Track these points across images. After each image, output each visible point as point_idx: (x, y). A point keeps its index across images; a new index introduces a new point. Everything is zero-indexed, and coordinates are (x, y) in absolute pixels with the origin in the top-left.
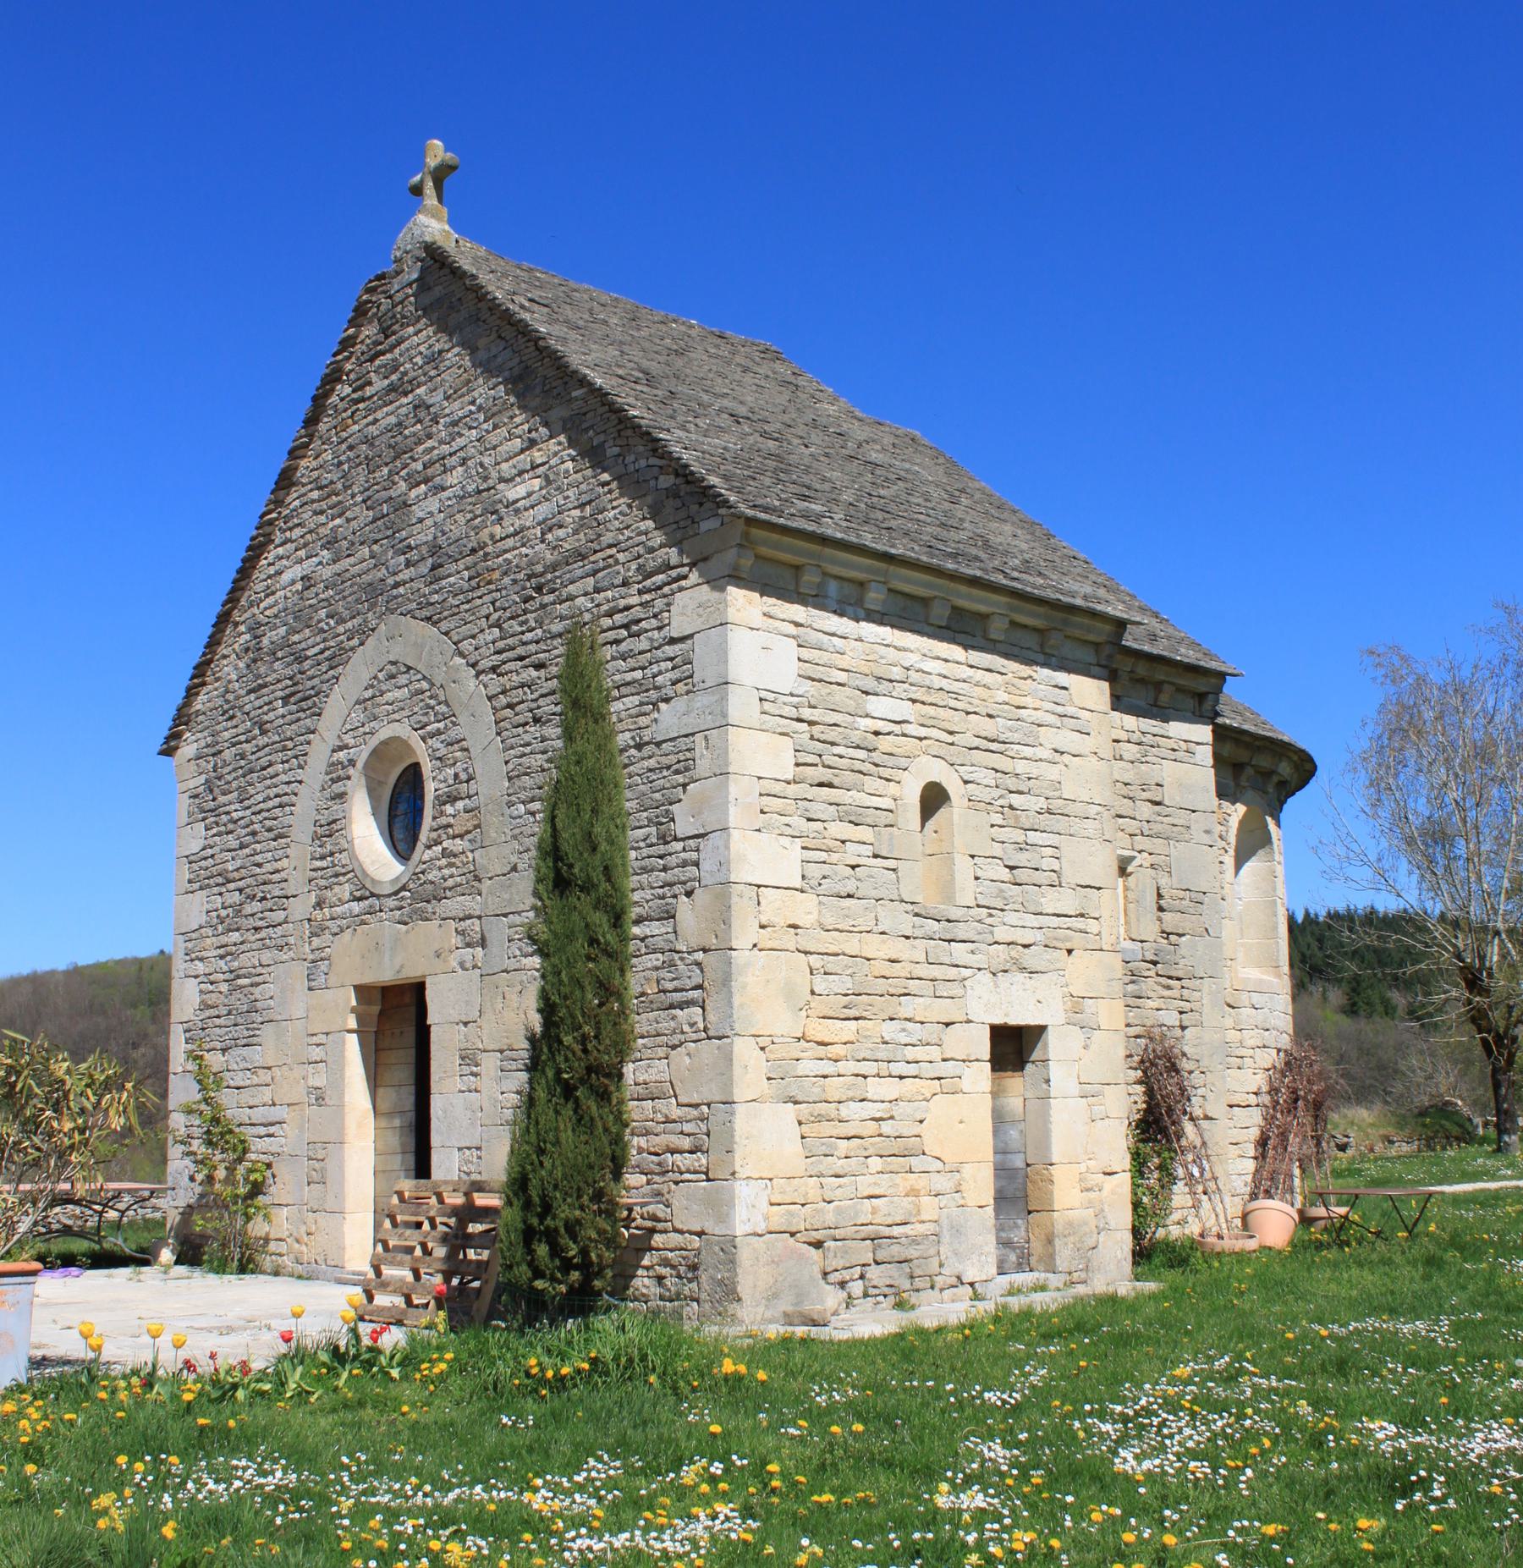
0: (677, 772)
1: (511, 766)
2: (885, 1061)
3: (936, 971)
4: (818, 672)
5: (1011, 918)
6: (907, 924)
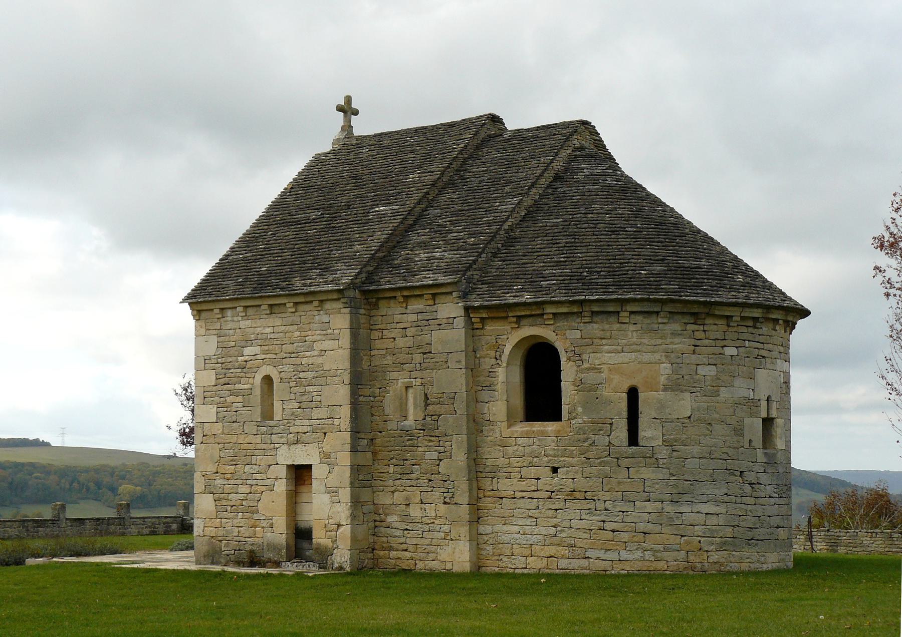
3: (265, 446)
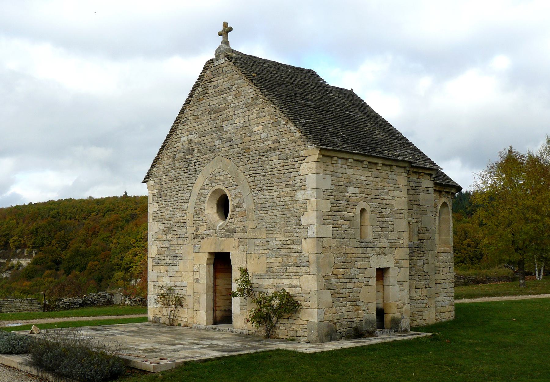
0: (302, 209)
1: (255, 201)
2: (350, 278)
3: (363, 256)
4: (336, 183)
5: (381, 241)
6: (356, 244)
